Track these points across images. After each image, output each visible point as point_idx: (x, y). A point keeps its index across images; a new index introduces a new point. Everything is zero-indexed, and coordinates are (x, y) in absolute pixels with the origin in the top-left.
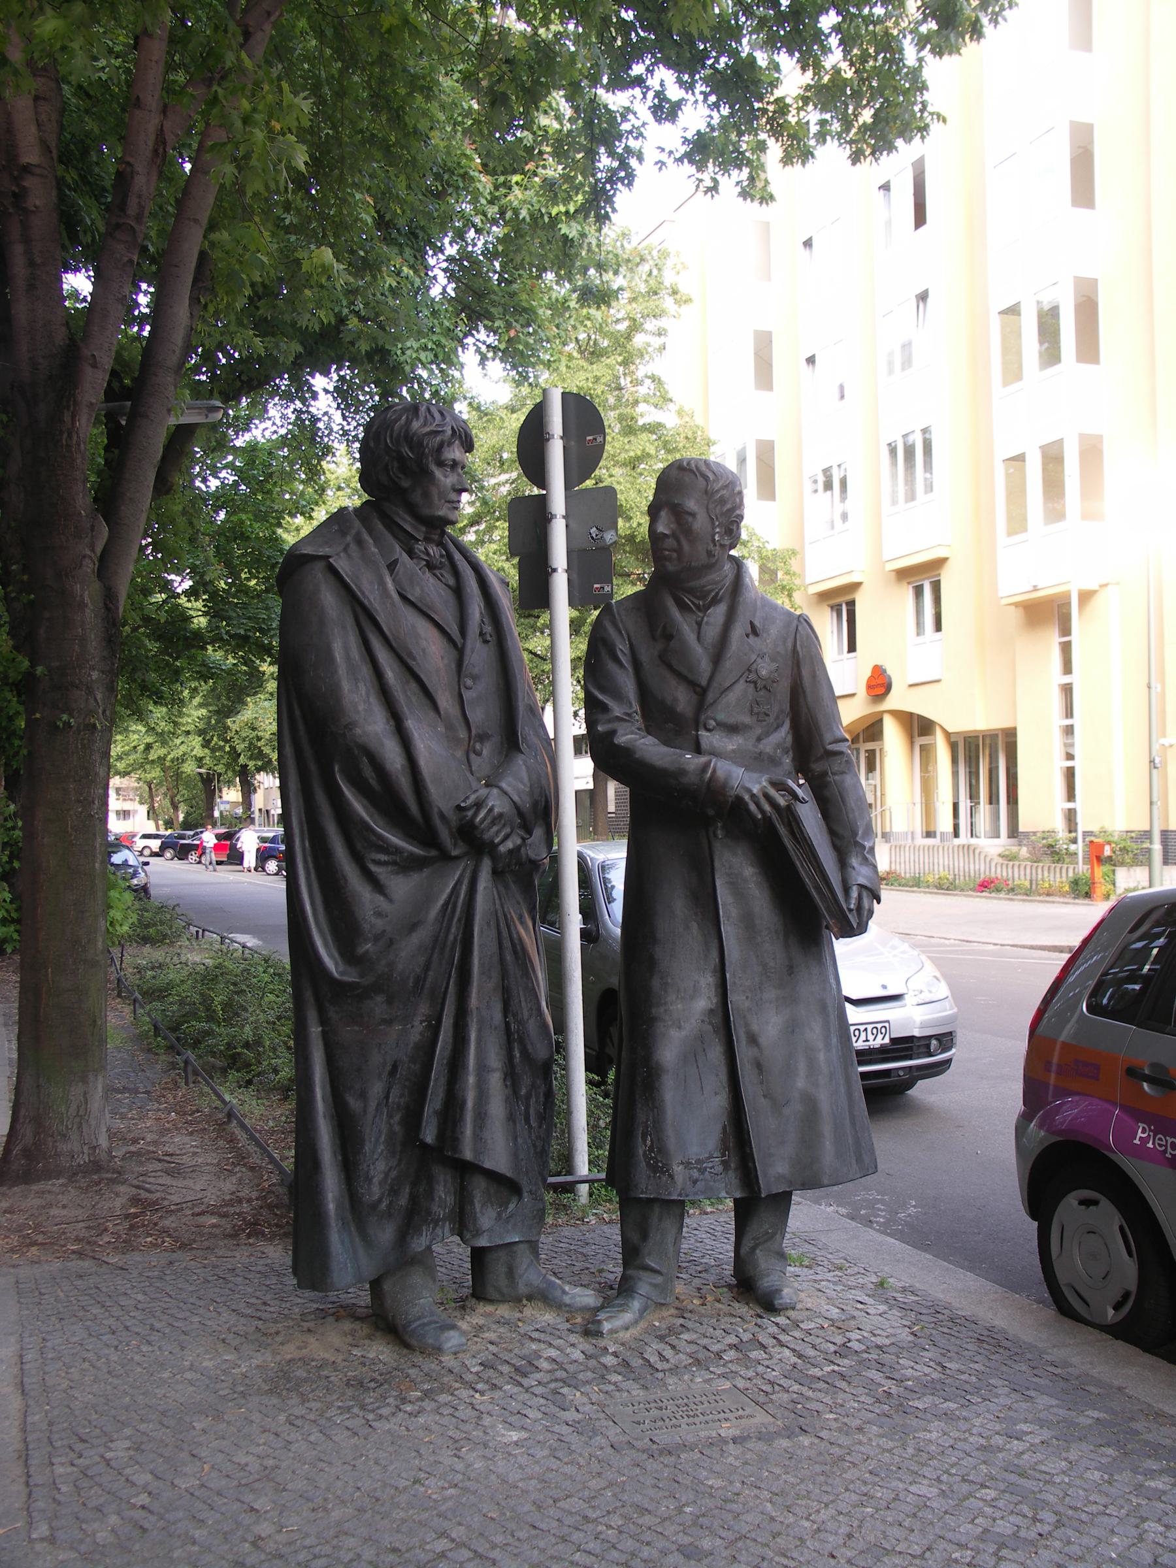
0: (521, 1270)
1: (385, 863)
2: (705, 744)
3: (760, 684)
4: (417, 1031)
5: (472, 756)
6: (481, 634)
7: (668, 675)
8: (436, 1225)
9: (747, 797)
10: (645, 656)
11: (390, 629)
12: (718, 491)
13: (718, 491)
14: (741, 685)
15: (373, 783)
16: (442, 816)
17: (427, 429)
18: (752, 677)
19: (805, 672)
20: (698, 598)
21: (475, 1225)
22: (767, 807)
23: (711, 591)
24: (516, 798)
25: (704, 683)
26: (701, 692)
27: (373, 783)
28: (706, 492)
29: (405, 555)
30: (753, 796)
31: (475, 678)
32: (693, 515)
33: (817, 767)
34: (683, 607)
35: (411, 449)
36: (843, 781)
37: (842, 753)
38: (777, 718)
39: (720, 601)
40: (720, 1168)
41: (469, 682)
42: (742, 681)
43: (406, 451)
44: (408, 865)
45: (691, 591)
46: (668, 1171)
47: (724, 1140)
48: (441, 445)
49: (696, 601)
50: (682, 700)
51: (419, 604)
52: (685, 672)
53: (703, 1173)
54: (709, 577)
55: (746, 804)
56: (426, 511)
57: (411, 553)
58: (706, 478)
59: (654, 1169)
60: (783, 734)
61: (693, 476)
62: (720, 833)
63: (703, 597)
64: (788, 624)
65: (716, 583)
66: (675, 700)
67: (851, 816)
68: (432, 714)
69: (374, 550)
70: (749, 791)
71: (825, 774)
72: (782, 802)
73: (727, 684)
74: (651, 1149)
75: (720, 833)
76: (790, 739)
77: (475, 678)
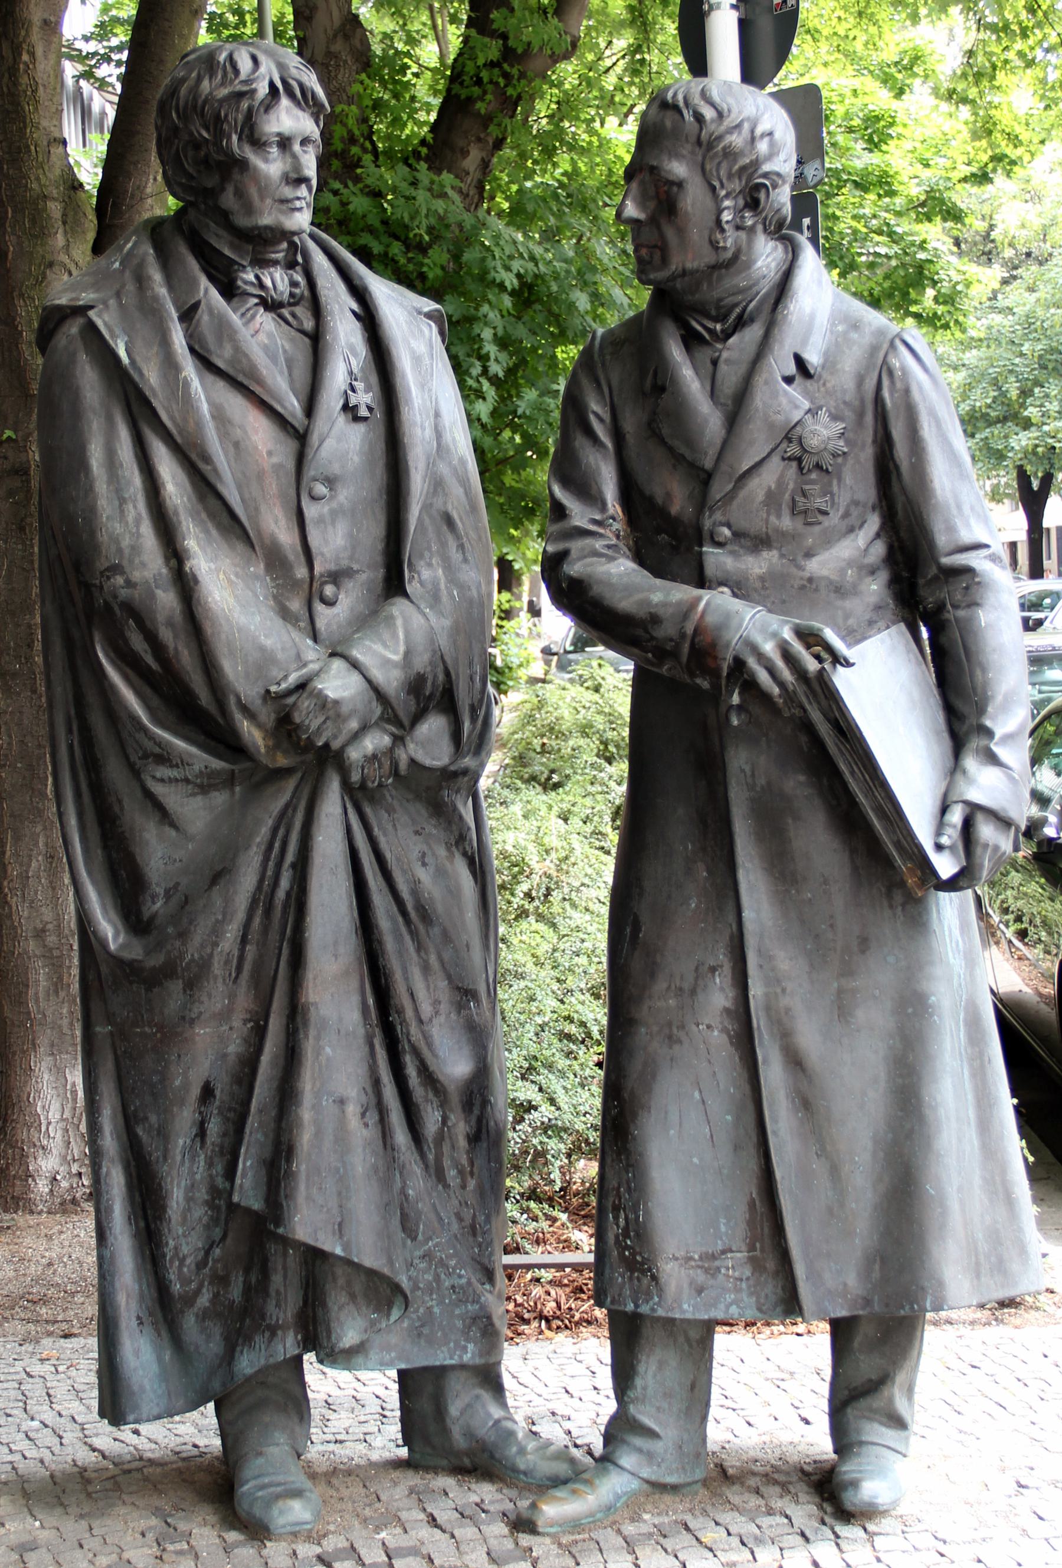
0: (454, 1409)
1: (171, 781)
3: (808, 462)
5: (319, 608)
6: (348, 408)
8: (273, 1334)
9: (752, 662)
10: (630, 425)
11: (172, 418)
12: (720, 138)
15: (149, 660)
16: (245, 709)
17: (224, 92)
18: (793, 449)
19: (898, 432)
20: (716, 320)
21: (329, 1337)
23: (736, 305)
24: (378, 675)
25: (708, 464)
26: (703, 479)
27: (149, 660)
28: (699, 142)
29: (214, 293)
30: (761, 657)
31: (330, 482)
32: (680, 184)
34: (691, 340)
38: (846, 515)
39: (752, 320)
41: (320, 489)
42: (776, 459)
44: (206, 784)
46: (650, 1270)
47: (751, 1223)
48: (250, 114)
49: (710, 325)
50: (675, 495)
51: (231, 371)
52: (683, 450)
53: (713, 1276)
56: (242, 221)
57: (230, 291)
58: (699, 118)
61: (677, 116)
63: (722, 318)
64: (874, 349)
65: (741, 291)
66: (668, 495)
68: (240, 547)
69: (163, 291)
71: (941, 607)
72: (812, 665)
73: (745, 467)
74: (626, 1234)
76: (879, 549)
77: (330, 482)
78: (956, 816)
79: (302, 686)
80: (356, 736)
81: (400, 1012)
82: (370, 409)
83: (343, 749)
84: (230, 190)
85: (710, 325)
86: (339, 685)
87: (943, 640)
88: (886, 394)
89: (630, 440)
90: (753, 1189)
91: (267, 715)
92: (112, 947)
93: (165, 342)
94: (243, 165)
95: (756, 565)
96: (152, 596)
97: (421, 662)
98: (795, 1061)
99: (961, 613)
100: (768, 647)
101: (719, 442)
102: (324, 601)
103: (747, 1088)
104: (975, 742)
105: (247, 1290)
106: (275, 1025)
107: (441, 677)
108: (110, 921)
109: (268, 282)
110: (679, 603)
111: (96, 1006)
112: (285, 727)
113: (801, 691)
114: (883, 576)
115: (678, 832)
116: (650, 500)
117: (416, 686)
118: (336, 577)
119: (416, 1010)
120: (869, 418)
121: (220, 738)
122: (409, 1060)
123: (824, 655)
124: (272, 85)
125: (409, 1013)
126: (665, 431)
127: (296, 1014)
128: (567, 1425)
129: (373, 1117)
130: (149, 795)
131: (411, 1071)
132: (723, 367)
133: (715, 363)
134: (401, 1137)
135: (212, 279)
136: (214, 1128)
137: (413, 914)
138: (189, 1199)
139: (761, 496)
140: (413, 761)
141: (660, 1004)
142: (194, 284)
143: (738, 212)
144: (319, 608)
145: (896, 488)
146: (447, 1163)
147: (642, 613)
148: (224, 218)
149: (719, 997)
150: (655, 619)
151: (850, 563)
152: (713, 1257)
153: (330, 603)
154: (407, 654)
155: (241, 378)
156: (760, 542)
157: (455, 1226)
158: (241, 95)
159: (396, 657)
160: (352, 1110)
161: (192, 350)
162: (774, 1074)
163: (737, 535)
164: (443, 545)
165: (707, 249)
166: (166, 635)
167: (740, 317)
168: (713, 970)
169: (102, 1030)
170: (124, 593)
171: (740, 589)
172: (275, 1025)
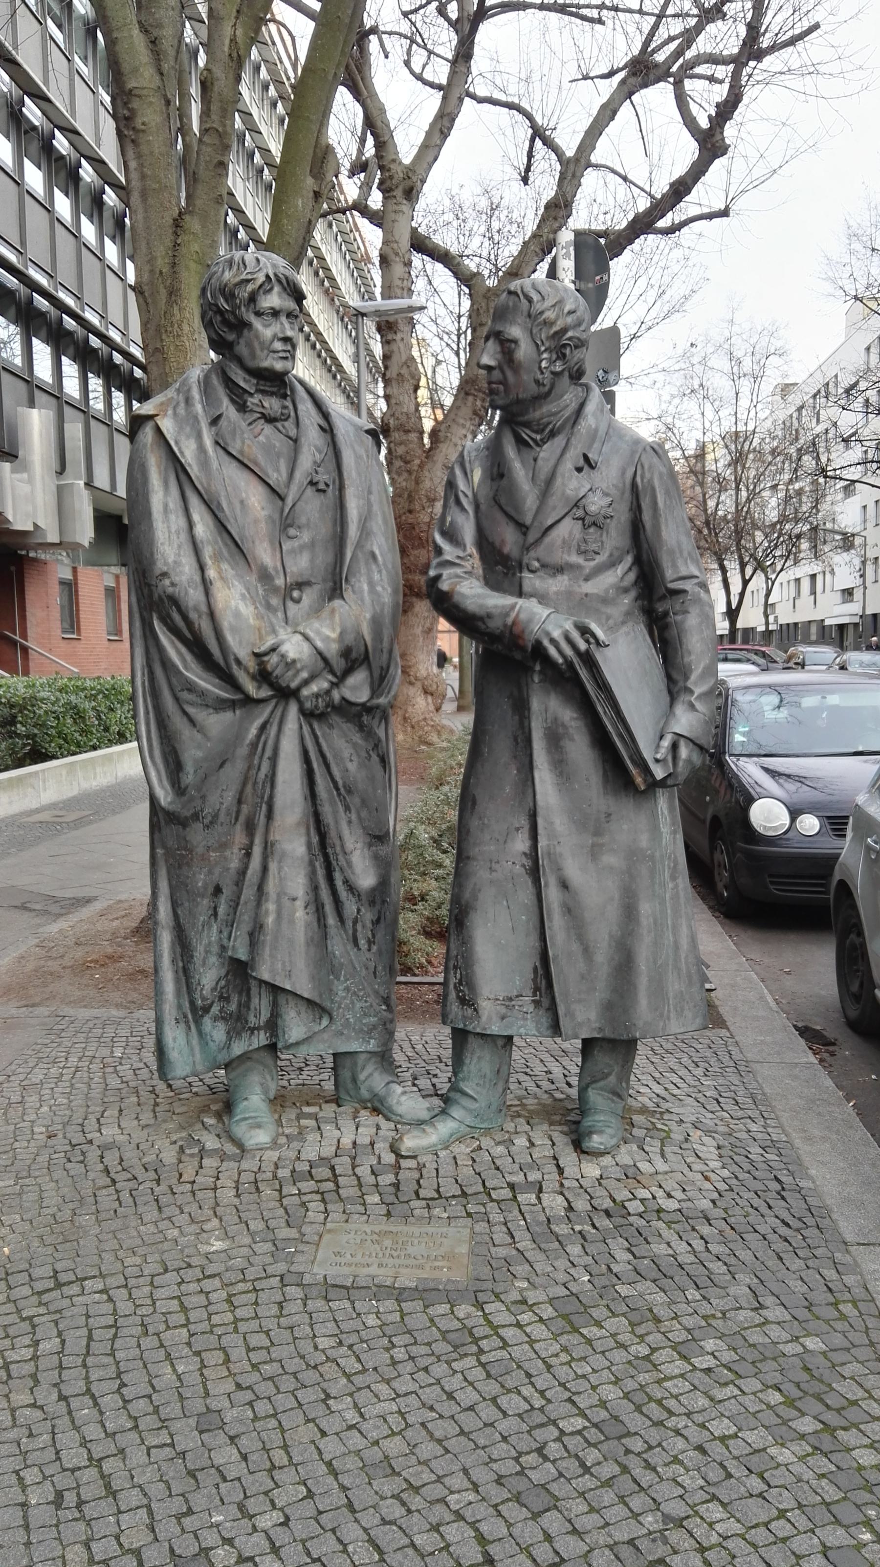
0: (362, 1077)
2: (526, 587)
4: (235, 864)
7: (499, 515)
9: (546, 643)
12: (542, 313)
13: (542, 313)
14: (567, 523)
16: (238, 662)
17: (237, 279)
18: (580, 513)
20: (537, 432)
22: (569, 651)
24: (319, 644)
28: (529, 316)
30: (553, 641)
32: (515, 342)
33: (660, 608)
34: (521, 442)
35: (227, 301)
36: (683, 622)
37: (684, 592)
40: (531, 1008)
43: (222, 302)
44: (221, 705)
45: (527, 425)
49: (534, 436)
50: (508, 539)
54: (544, 409)
55: (545, 649)
56: (251, 364)
57: (242, 408)
58: (530, 300)
59: (463, 1001)
60: (622, 573)
62: (536, 679)
63: (539, 431)
67: (686, 660)
70: (548, 634)
71: (666, 614)
72: (582, 646)
73: (549, 522)
74: (460, 983)
75: (536, 679)
76: (632, 576)
78: (666, 743)
79: (273, 650)
80: (306, 682)
81: (333, 847)
82: (327, 485)
83: (299, 689)
84: (242, 341)
85: (534, 436)
86: (294, 647)
87: (666, 635)
88: (638, 479)
89: (483, 507)
90: (532, 961)
91: (252, 665)
92: (163, 803)
93: (199, 437)
94: (248, 325)
95: (556, 585)
96: (186, 593)
97: (350, 639)
98: (564, 885)
99: (679, 618)
100: (556, 634)
101: (535, 507)
102: (292, 599)
103: (536, 902)
104: (684, 697)
105: (240, 1005)
106: (257, 851)
107: (363, 649)
108: (163, 787)
109: (266, 404)
110: (503, 607)
111: (156, 836)
112: (263, 676)
113: (576, 661)
114: (633, 594)
115: (501, 749)
116: (492, 544)
117: (346, 653)
118: (300, 585)
119: (342, 846)
120: (628, 494)
121: (227, 678)
122: (337, 876)
123: (592, 640)
124: (268, 276)
125: (338, 849)
126: (503, 502)
127: (268, 848)
128: (435, 1080)
129: (312, 908)
130: (185, 713)
131: (339, 883)
132: (540, 462)
133: (535, 460)
134: (331, 920)
135: (233, 401)
136: (221, 910)
137: (342, 790)
138: (207, 952)
139: (559, 542)
140: (343, 699)
141: (486, 848)
142: (220, 403)
143: (552, 362)
144: (290, 604)
145: (642, 536)
146: (360, 935)
147: (481, 612)
148: (240, 361)
149: (521, 844)
150: (489, 616)
151: (612, 586)
152: (511, 999)
153: (298, 601)
154: (341, 633)
155: (246, 461)
156: (559, 570)
157: (364, 972)
158: (248, 281)
159: (334, 635)
160: (300, 904)
161: (217, 443)
162: (553, 894)
163: (544, 566)
164: (369, 570)
165: (533, 385)
166: (193, 616)
167: (552, 431)
168: (518, 829)
169: (160, 851)
170: (170, 590)
171: (543, 599)
172: (257, 851)
